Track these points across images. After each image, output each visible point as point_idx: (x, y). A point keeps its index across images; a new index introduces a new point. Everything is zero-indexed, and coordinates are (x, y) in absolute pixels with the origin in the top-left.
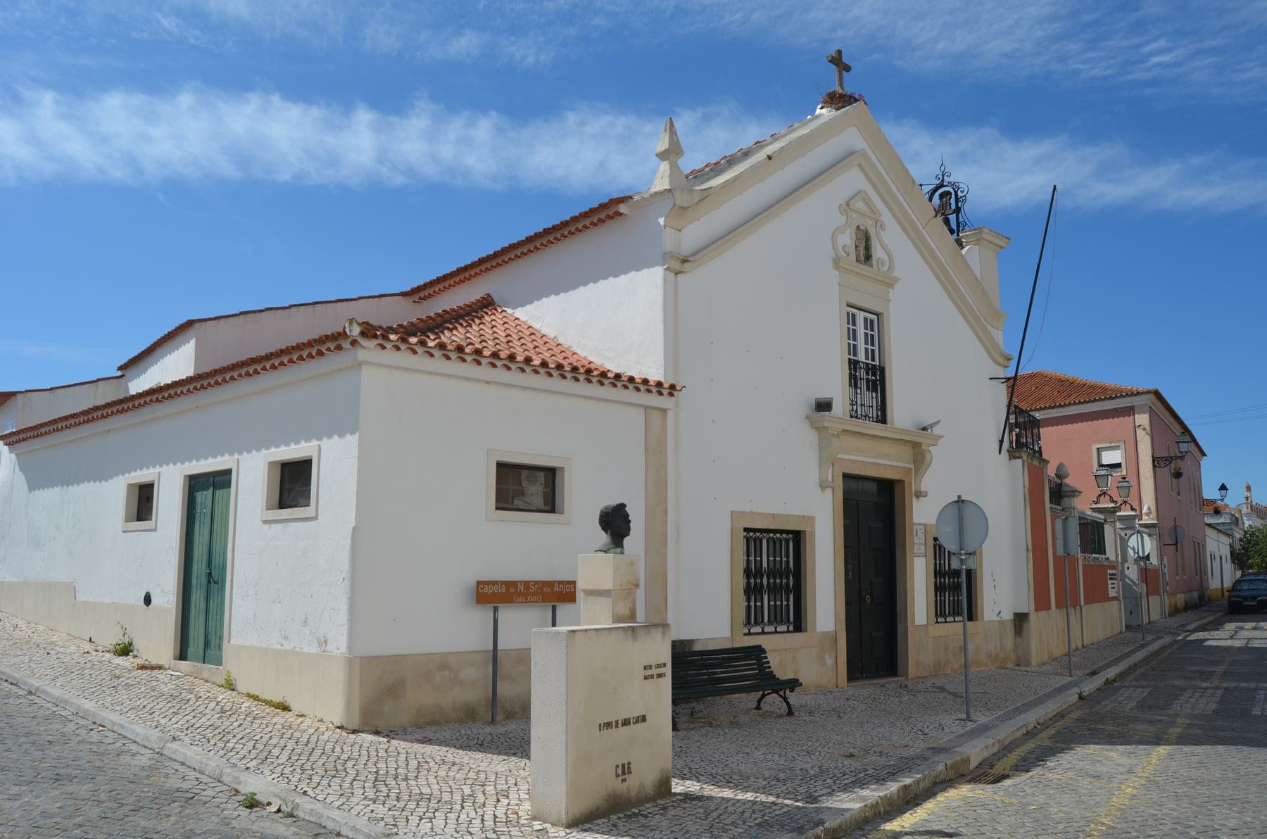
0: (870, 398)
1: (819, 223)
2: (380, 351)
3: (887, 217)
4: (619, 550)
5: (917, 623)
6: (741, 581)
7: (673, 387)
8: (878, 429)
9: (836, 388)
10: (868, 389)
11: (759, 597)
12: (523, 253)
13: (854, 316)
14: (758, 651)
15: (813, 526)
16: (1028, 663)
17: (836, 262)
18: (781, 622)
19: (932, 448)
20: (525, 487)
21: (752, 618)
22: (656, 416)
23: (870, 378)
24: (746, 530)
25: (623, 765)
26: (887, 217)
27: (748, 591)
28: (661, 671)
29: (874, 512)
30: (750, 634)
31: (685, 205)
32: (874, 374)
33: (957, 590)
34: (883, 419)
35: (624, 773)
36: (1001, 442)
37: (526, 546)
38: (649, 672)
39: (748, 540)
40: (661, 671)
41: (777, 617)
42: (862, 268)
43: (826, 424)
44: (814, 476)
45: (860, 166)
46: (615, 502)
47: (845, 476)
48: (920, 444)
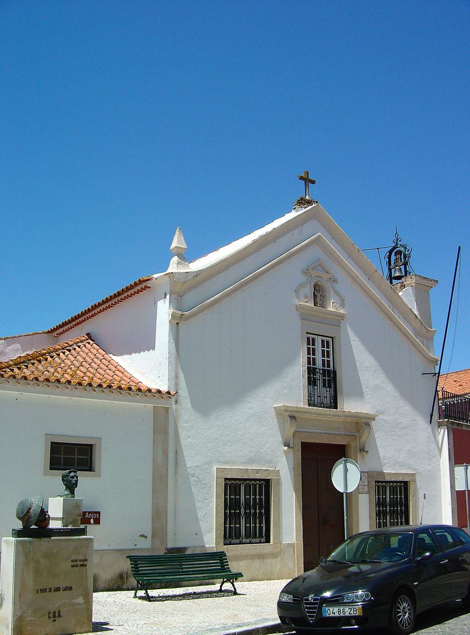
0: (323, 392)
6: (374, 509)
10: (324, 386)
12: (115, 302)
13: (313, 340)
24: (226, 479)
27: (378, 514)
32: (329, 376)
35: (54, 616)
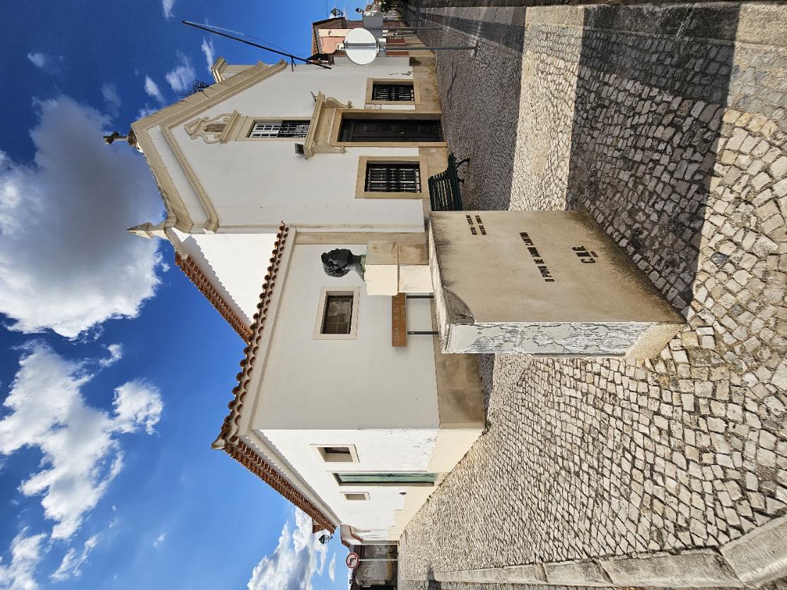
1: (198, 150)
2: (241, 421)
3: (201, 116)
4: (362, 259)
5: (414, 109)
7: (282, 228)
8: (314, 125)
9: (290, 143)
10: (294, 129)
11: (401, 186)
13: (255, 135)
14: (432, 181)
15: (365, 157)
16: (434, 59)
17: (223, 141)
18: (414, 173)
19: (326, 97)
20: (336, 318)
21: (413, 189)
22: (300, 238)
23: (288, 128)
24: (366, 190)
25: (579, 255)
26: (201, 116)
28: (474, 220)
29: (355, 127)
30: (420, 190)
31: (175, 221)
33: (398, 91)
34: (308, 122)
36: (325, 67)
37: (371, 322)
38: (478, 230)
39: (371, 190)
40: (474, 220)
41: (412, 176)
42: (227, 130)
43: (309, 148)
44: (339, 156)
45: (170, 128)
46: (320, 264)
47: (340, 139)
48: (323, 104)
